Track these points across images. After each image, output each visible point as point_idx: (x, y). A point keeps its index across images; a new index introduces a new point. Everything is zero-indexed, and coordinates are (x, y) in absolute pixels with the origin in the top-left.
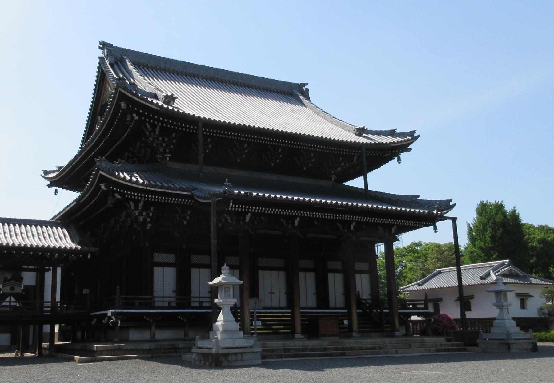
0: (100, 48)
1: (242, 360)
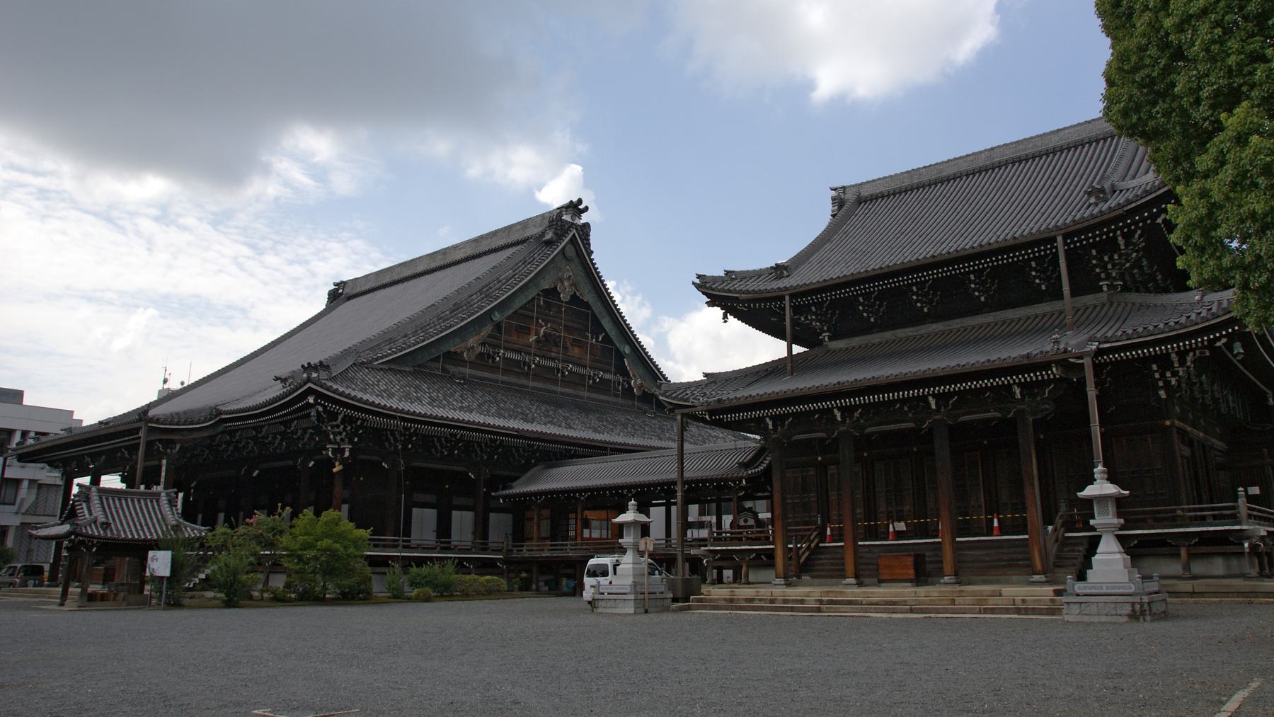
1: (1133, 604)
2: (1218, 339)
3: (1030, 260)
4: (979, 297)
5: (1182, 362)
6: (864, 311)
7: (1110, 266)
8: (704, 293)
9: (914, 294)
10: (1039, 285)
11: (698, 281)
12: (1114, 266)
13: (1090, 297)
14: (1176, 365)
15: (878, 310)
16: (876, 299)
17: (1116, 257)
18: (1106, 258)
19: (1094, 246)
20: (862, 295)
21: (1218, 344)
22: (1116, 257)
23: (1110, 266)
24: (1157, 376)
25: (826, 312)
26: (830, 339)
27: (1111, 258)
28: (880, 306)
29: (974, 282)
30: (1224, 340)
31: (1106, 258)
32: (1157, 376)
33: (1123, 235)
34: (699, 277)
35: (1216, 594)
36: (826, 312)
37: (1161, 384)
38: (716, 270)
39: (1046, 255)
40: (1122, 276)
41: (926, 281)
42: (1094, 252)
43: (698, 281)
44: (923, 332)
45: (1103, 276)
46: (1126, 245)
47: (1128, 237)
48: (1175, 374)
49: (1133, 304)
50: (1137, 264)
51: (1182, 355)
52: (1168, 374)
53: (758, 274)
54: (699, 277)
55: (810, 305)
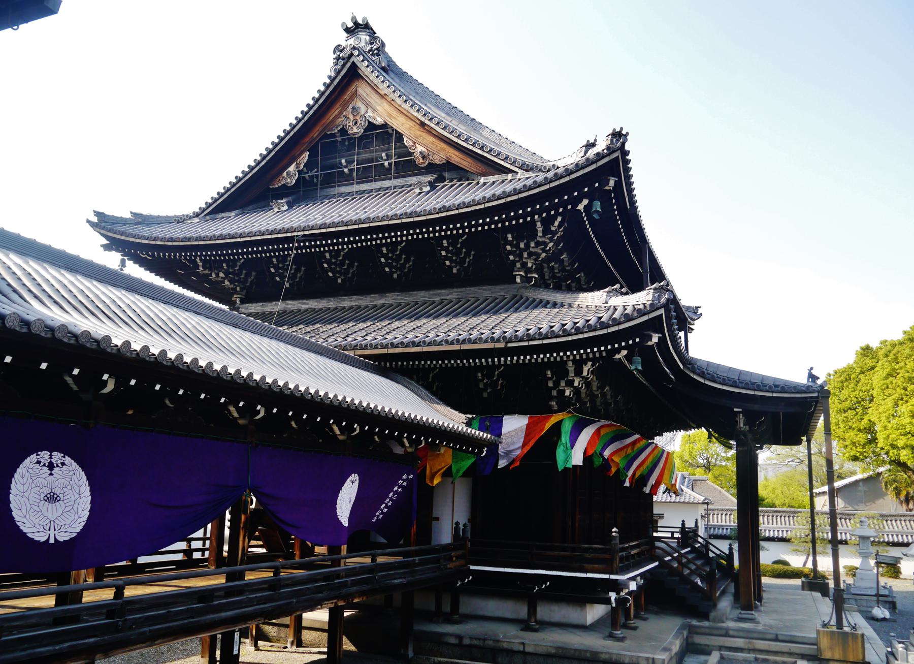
0: (347, 30)
2: (618, 351)
3: (441, 238)
4: (450, 267)
5: (579, 372)
6: (387, 264)
7: (525, 255)
8: (102, 235)
9: (443, 248)
10: (450, 267)
11: (95, 219)
12: (530, 255)
13: (422, 293)
14: (572, 374)
15: (403, 266)
16: (242, 267)
17: (532, 244)
18: (522, 245)
19: (510, 229)
20: (446, 237)
21: (617, 356)
22: (532, 244)
23: (525, 255)
24: (550, 384)
25: (342, 263)
26: (243, 302)
27: (527, 246)
28: (468, 254)
29: (446, 249)
30: (624, 352)
31: (522, 245)
32: (550, 384)
33: (543, 221)
34: (97, 214)
35: (791, 654)
36: (342, 263)
37: (554, 393)
38: (120, 209)
39: (402, 241)
40: (539, 269)
41: (397, 242)
42: (510, 237)
43: (95, 219)
44: (487, 294)
45: (518, 265)
46: (545, 233)
47: (548, 222)
48: (570, 383)
49: (534, 300)
50: (554, 256)
51: (579, 365)
52: (563, 383)
53: (180, 220)
54: (97, 214)
55: (222, 262)
